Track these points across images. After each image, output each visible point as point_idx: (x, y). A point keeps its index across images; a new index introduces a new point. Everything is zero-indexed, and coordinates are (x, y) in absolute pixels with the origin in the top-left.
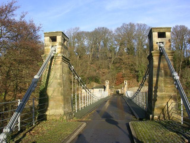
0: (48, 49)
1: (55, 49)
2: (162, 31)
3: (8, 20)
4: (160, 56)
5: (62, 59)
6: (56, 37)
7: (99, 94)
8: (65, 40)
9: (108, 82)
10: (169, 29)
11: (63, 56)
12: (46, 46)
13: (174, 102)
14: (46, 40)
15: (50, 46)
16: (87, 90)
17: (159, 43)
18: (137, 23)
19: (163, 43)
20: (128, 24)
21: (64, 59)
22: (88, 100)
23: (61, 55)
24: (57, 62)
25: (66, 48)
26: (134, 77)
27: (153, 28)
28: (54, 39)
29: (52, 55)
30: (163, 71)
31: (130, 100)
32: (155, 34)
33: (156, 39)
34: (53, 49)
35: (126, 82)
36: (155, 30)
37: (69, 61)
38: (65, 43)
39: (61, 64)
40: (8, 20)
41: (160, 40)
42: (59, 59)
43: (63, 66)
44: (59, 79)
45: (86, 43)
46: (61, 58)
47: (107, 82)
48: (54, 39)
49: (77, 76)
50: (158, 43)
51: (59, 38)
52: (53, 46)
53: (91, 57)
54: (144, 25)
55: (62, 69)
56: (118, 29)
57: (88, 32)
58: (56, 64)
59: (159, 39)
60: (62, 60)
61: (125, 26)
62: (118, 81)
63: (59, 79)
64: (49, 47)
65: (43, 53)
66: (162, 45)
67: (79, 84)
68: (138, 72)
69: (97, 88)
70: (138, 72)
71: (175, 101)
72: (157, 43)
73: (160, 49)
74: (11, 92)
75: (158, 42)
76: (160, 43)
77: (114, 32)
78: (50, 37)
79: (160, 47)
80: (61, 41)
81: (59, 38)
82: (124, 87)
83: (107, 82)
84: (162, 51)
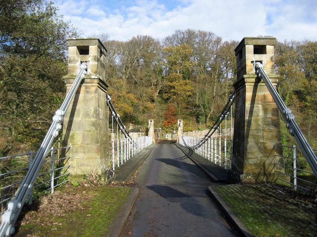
0: (74, 68)
1: (86, 67)
2: (260, 43)
3: (23, 17)
4: (255, 83)
5: (98, 84)
6: (88, 47)
7: (141, 142)
8: (101, 53)
9: (153, 121)
10: (272, 40)
11: (100, 79)
12: (70, 62)
13: (278, 155)
14: (72, 52)
15: (77, 61)
16: (127, 135)
17: (256, 61)
18: (199, 31)
19: (261, 62)
20: (184, 32)
21: (101, 83)
22: (125, 151)
23: (96, 77)
24: (90, 88)
25: (103, 66)
26: (191, 114)
27: (247, 38)
28: (84, 51)
29: (83, 76)
30: (260, 106)
31: (190, 151)
32: (249, 48)
33: (250, 56)
34: (83, 66)
35: (181, 123)
36: (249, 42)
37: (107, 86)
38: (102, 58)
39: (96, 91)
40: (23, 17)
41: (258, 57)
42: (93, 84)
43: (99, 95)
44: (93, 116)
45: (117, 61)
46: (96, 81)
47: (151, 121)
48: (84, 51)
49: (115, 113)
50: (253, 62)
51: (93, 50)
52: (81, 62)
53: (157, 81)
54: (210, 34)
55: (98, 100)
56: (167, 39)
57: (122, 43)
58: (87, 92)
59: (256, 55)
60: (97, 85)
61: (179, 36)
62: (168, 121)
63: (93, 116)
64: (76, 63)
65: (66, 74)
66: (260, 65)
67: (116, 125)
68: (199, 107)
69: (133, 131)
70: (199, 107)
71: (278, 153)
72: (252, 62)
73: (258, 71)
74: (308, 174)
75: (254, 60)
76: (257, 63)
77: (161, 44)
78: (78, 47)
79: (257, 69)
80: (96, 55)
81: (93, 50)
82: (177, 129)
83: (151, 121)
84: (260, 75)
